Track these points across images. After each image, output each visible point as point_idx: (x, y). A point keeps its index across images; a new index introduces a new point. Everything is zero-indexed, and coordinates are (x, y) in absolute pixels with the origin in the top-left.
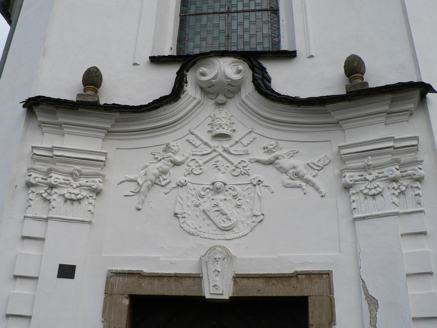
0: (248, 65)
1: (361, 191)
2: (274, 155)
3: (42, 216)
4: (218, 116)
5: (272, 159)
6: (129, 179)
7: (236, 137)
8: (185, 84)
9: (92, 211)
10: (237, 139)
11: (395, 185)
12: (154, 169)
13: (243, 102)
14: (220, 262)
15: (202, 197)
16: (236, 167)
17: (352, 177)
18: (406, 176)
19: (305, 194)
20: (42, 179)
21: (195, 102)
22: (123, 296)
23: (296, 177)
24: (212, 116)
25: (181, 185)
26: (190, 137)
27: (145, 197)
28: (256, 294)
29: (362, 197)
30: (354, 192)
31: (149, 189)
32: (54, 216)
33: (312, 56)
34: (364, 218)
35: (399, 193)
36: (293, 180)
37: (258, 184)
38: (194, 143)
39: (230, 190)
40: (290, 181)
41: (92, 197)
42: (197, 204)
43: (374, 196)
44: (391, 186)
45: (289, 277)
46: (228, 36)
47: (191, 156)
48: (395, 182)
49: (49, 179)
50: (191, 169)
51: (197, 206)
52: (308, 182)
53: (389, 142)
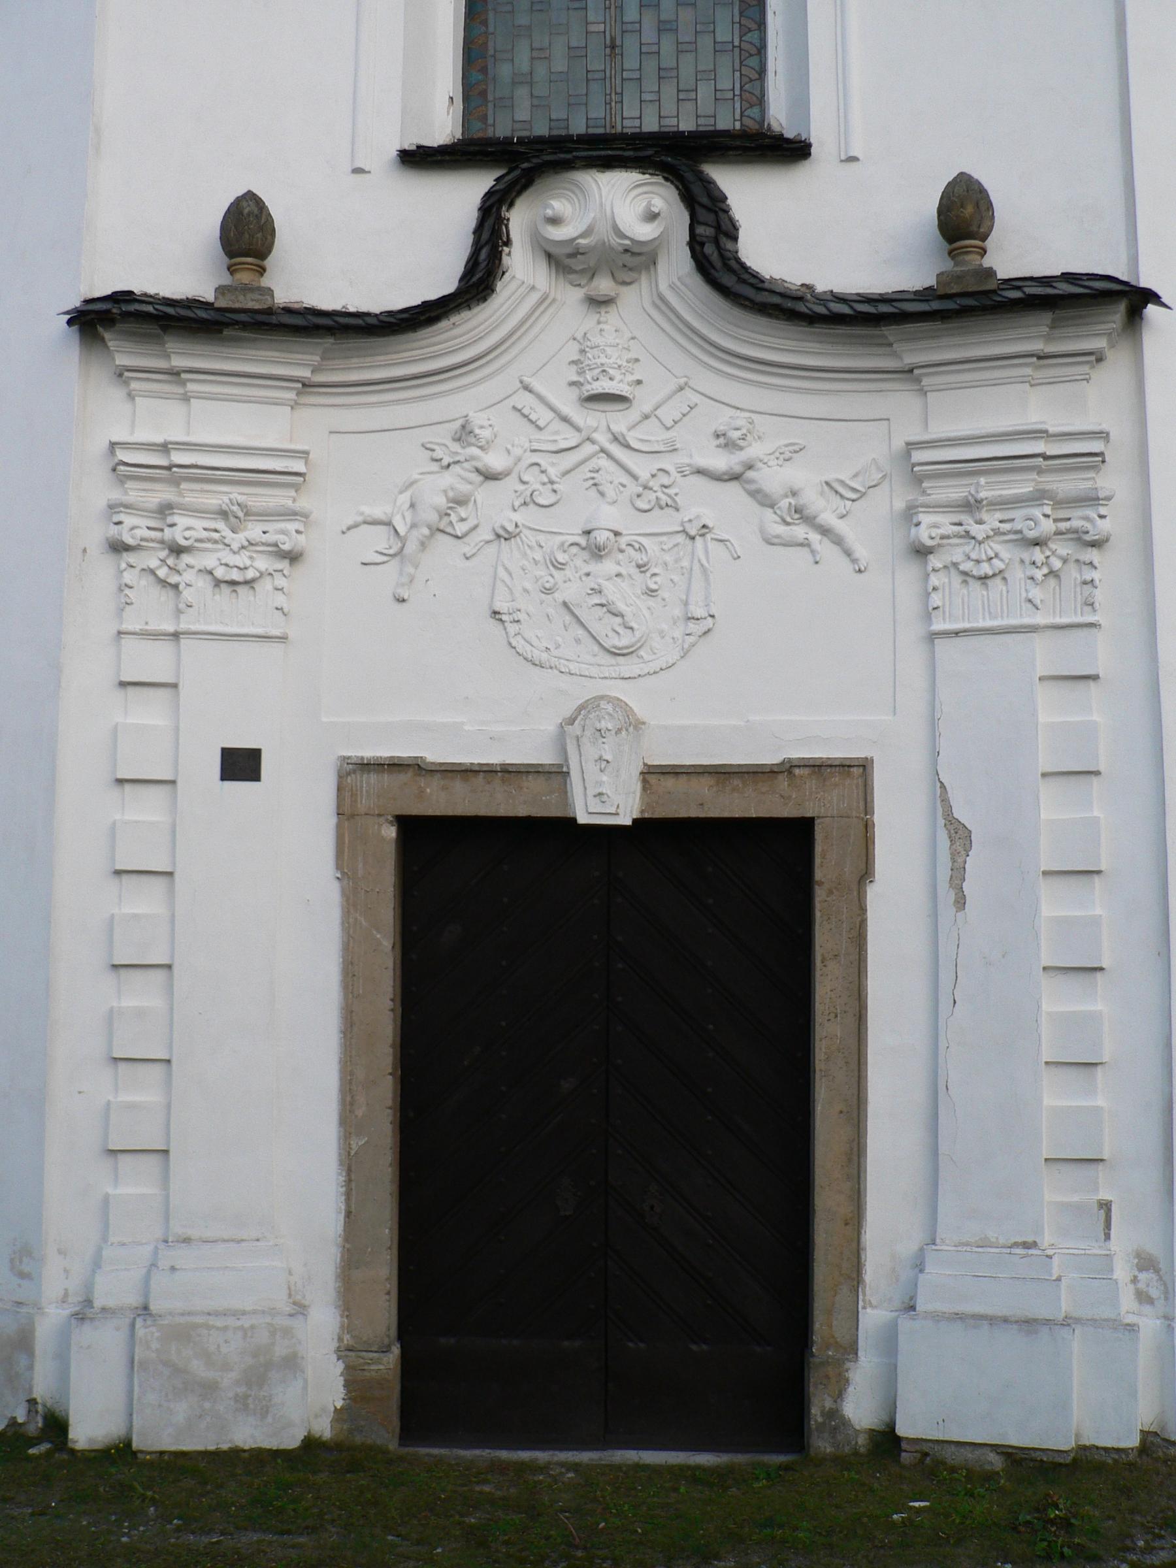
0: (677, 192)
1: (955, 565)
2: (742, 456)
3: (162, 627)
4: (596, 340)
5: (738, 469)
6: (369, 519)
7: (644, 401)
8: (506, 249)
9: (286, 610)
10: (647, 409)
11: (1038, 555)
12: (435, 489)
13: (662, 298)
14: (611, 739)
15: (559, 566)
16: (646, 487)
17: (935, 526)
18: (1069, 531)
19: (817, 563)
20: (148, 528)
21: (535, 297)
22: (382, 819)
23: (797, 516)
24: (579, 336)
25: (503, 536)
26: (525, 400)
27: (416, 567)
28: (694, 813)
29: (957, 579)
30: (939, 565)
31: (423, 545)
32: (193, 628)
33: (853, 159)
34: (957, 633)
35: (1045, 576)
36: (788, 524)
37: (703, 535)
38: (533, 417)
39: (630, 550)
40: (781, 529)
41: (281, 571)
42: (547, 585)
43: (984, 578)
44: (1026, 556)
45: (772, 772)
46: (613, 47)
47: (528, 454)
48: (1038, 548)
49: (167, 530)
50: (530, 490)
51: (547, 591)
52: (825, 531)
53: (1033, 442)
